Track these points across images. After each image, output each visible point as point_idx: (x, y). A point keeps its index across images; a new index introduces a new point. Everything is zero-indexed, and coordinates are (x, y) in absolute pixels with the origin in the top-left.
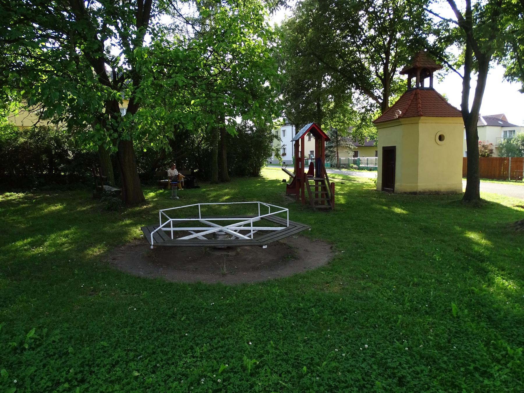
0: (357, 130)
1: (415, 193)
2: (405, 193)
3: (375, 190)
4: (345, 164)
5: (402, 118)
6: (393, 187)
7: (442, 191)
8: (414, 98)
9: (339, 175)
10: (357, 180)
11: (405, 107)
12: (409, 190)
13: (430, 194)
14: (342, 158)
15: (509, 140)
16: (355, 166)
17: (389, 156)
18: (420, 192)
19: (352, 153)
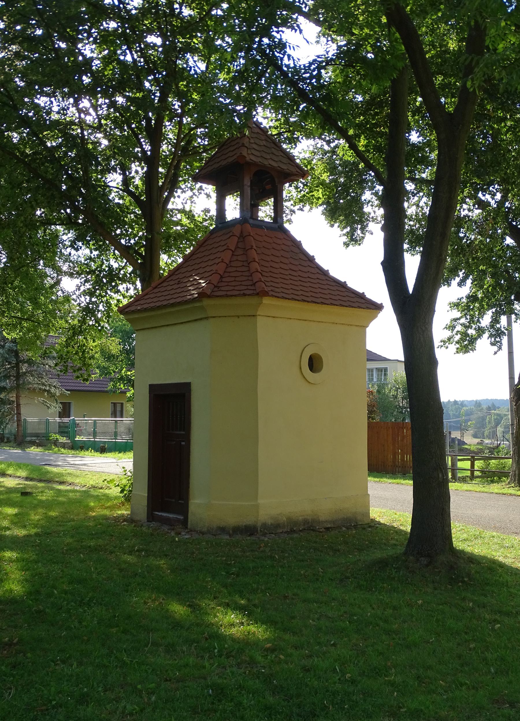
0: (70, 339)
1: (249, 530)
2: (223, 530)
3: (125, 519)
4: (37, 435)
5: (209, 297)
6: (184, 510)
7: (322, 518)
8: (237, 247)
9: (19, 466)
10: (69, 479)
11: (214, 268)
12: (232, 520)
13: (292, 531)
14: (29, 419)
15: (381, 387)
16: (63, 440)
17: (169, 420)
18: (264, 525)
19: (56, 408)
